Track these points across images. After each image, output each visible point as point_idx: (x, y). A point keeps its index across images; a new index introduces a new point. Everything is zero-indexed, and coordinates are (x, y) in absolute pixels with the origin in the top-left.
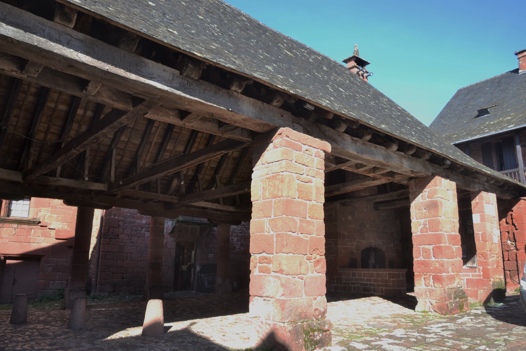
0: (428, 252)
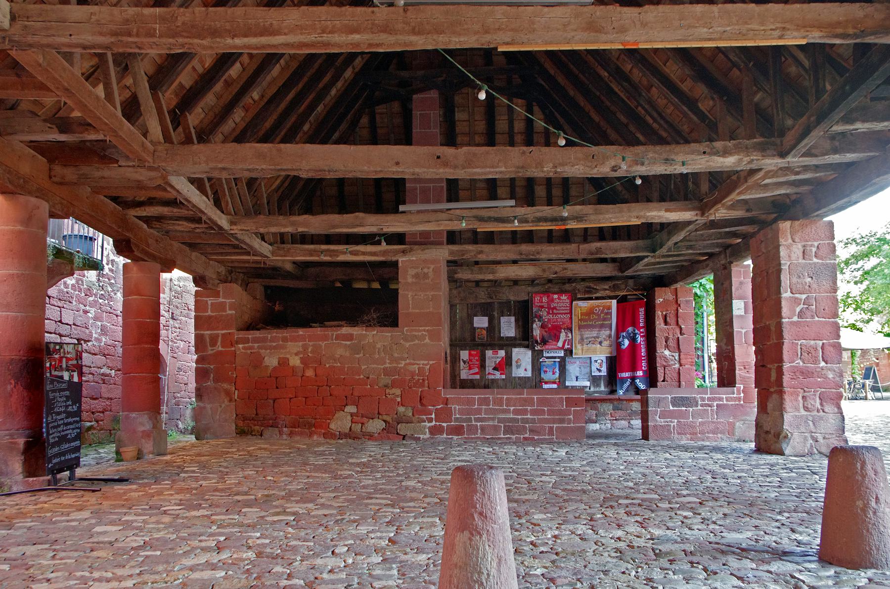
0: (813, 353)
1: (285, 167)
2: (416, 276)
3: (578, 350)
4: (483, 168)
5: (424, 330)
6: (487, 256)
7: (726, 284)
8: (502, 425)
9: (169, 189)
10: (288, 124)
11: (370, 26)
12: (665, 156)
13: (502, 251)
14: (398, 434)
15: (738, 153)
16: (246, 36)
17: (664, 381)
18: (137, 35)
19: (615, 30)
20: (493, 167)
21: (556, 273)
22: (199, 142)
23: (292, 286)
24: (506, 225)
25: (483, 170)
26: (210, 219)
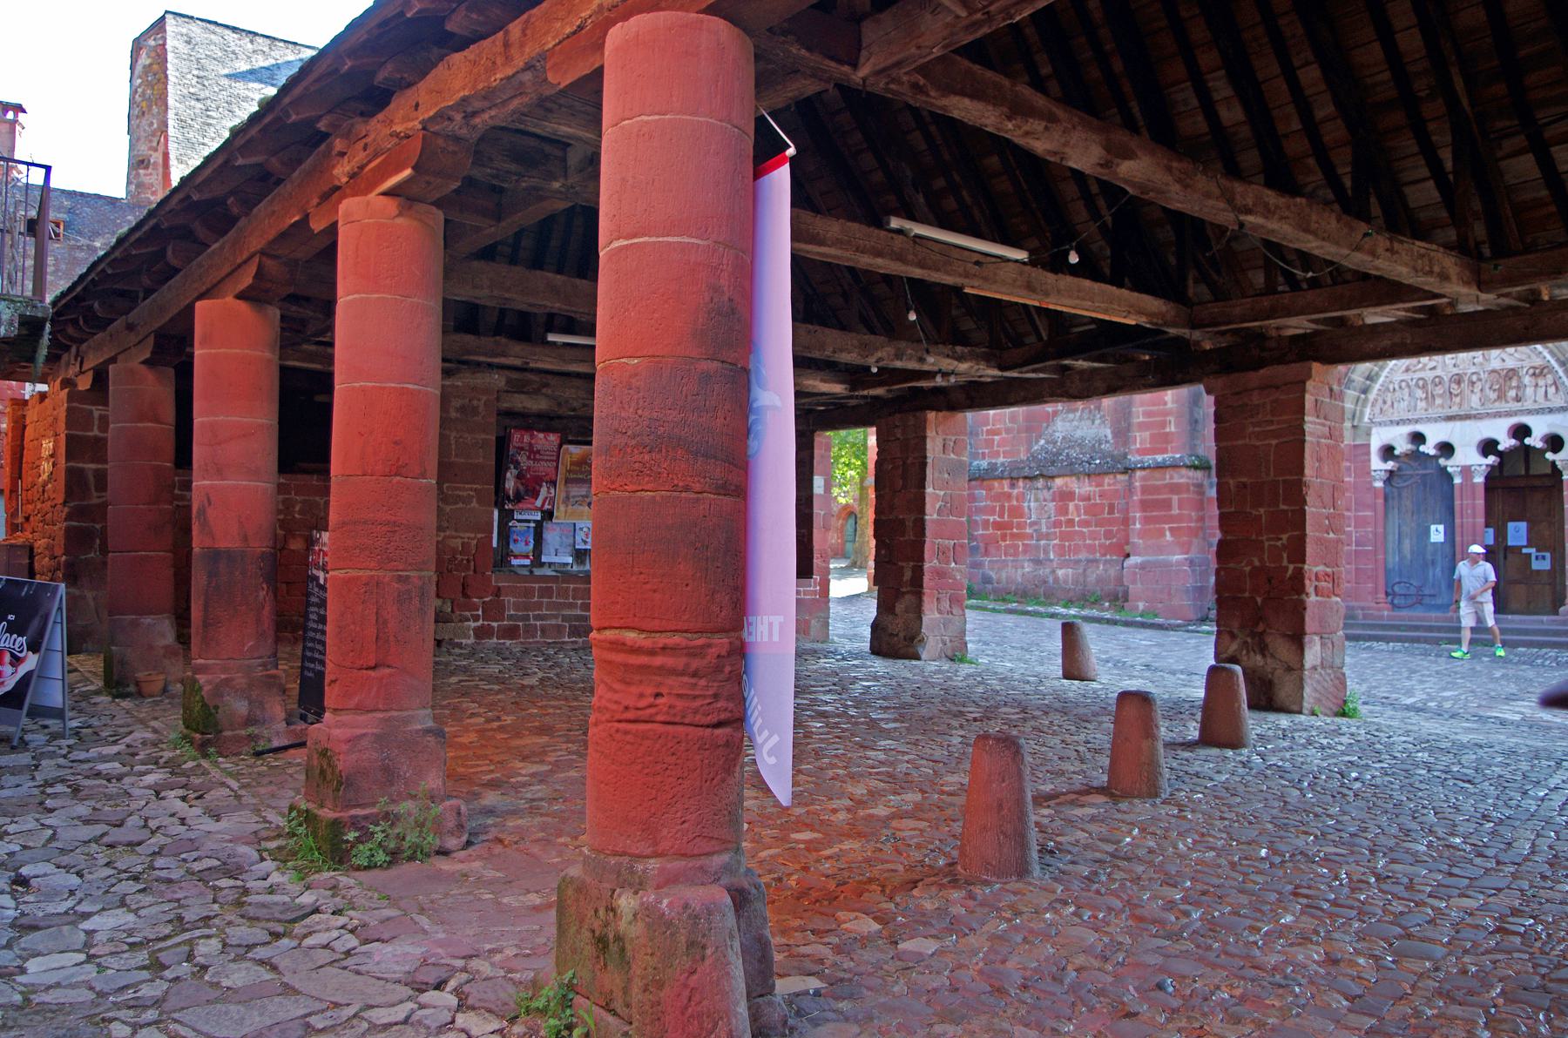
2: (462, 409)
3: (560, 512)
5: (471, 489)
12: (919, 354)
15: (971, 360)
21: (574, 410)
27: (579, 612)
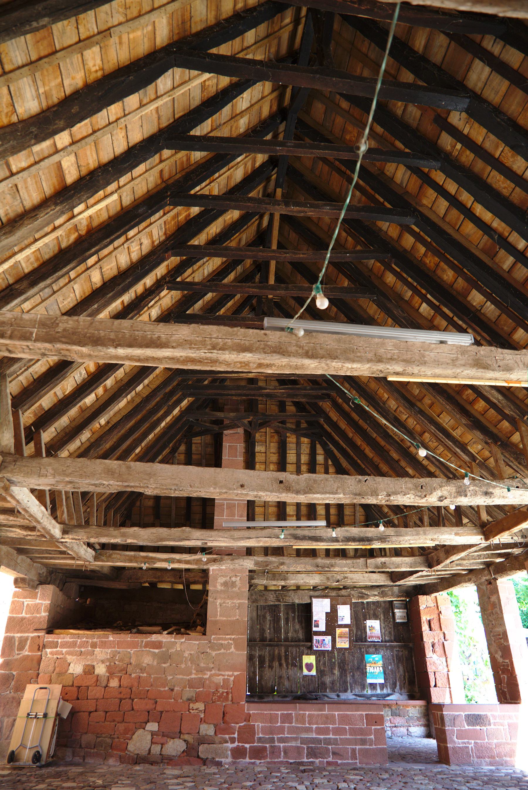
1: (132, 484)
2: (225, 584)
4: (323, 493)
5: (231, 639)
6: (288, 567)
7: (493, 598)
8: (305, 746)
9: (9, 499)
10: (124, 446)
11: (262, 346)
12: (484, 489)
13: (301, 563)
14: (198, 757)
16: (130, 346)
17: (435, 686)
18: (11, 337)
19: (501, 368)
20: (332, 493)
21: (338, 581)
22: (47, 456)
23: (105, 586)
24: (319, 543)
25: (323, 496)
26: (44, 528)
27: (314, 736)
